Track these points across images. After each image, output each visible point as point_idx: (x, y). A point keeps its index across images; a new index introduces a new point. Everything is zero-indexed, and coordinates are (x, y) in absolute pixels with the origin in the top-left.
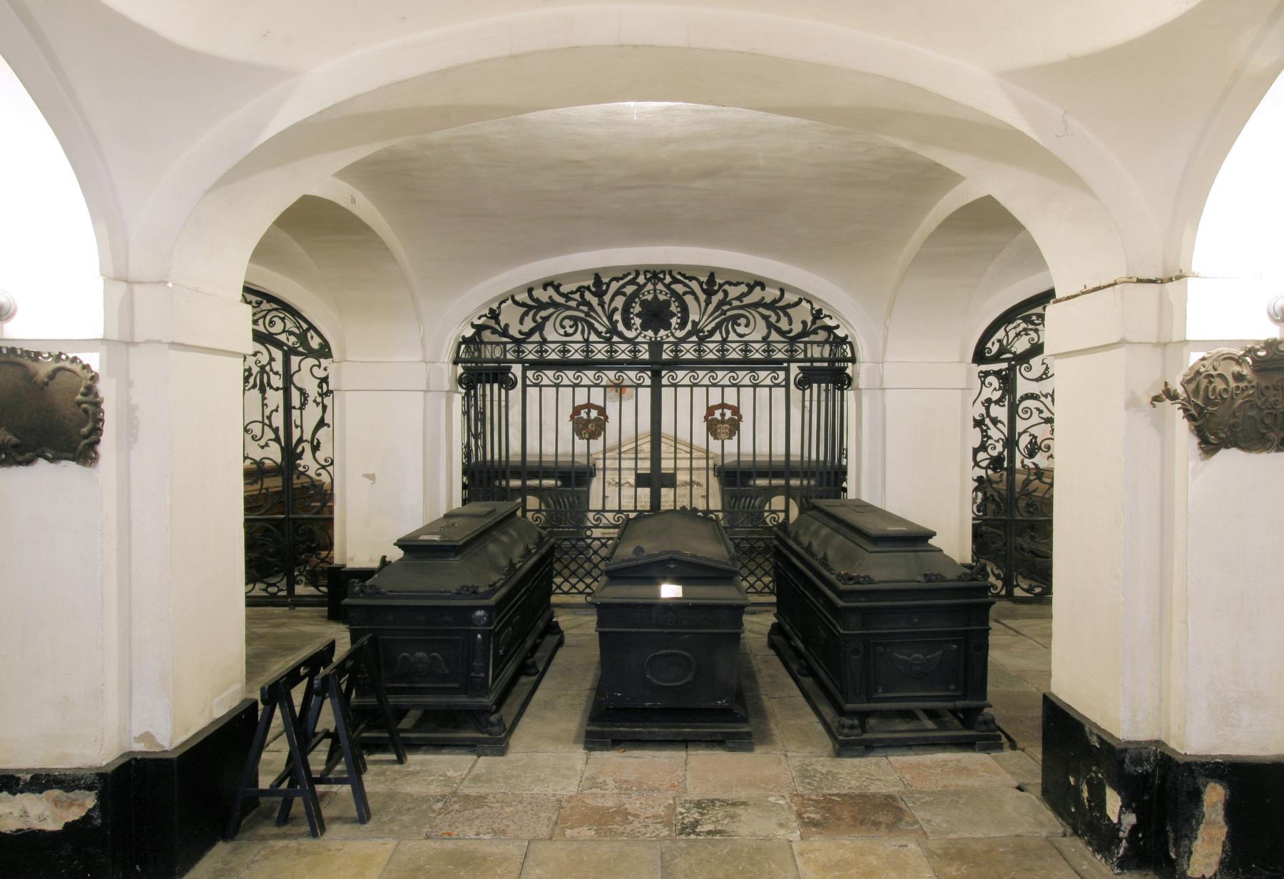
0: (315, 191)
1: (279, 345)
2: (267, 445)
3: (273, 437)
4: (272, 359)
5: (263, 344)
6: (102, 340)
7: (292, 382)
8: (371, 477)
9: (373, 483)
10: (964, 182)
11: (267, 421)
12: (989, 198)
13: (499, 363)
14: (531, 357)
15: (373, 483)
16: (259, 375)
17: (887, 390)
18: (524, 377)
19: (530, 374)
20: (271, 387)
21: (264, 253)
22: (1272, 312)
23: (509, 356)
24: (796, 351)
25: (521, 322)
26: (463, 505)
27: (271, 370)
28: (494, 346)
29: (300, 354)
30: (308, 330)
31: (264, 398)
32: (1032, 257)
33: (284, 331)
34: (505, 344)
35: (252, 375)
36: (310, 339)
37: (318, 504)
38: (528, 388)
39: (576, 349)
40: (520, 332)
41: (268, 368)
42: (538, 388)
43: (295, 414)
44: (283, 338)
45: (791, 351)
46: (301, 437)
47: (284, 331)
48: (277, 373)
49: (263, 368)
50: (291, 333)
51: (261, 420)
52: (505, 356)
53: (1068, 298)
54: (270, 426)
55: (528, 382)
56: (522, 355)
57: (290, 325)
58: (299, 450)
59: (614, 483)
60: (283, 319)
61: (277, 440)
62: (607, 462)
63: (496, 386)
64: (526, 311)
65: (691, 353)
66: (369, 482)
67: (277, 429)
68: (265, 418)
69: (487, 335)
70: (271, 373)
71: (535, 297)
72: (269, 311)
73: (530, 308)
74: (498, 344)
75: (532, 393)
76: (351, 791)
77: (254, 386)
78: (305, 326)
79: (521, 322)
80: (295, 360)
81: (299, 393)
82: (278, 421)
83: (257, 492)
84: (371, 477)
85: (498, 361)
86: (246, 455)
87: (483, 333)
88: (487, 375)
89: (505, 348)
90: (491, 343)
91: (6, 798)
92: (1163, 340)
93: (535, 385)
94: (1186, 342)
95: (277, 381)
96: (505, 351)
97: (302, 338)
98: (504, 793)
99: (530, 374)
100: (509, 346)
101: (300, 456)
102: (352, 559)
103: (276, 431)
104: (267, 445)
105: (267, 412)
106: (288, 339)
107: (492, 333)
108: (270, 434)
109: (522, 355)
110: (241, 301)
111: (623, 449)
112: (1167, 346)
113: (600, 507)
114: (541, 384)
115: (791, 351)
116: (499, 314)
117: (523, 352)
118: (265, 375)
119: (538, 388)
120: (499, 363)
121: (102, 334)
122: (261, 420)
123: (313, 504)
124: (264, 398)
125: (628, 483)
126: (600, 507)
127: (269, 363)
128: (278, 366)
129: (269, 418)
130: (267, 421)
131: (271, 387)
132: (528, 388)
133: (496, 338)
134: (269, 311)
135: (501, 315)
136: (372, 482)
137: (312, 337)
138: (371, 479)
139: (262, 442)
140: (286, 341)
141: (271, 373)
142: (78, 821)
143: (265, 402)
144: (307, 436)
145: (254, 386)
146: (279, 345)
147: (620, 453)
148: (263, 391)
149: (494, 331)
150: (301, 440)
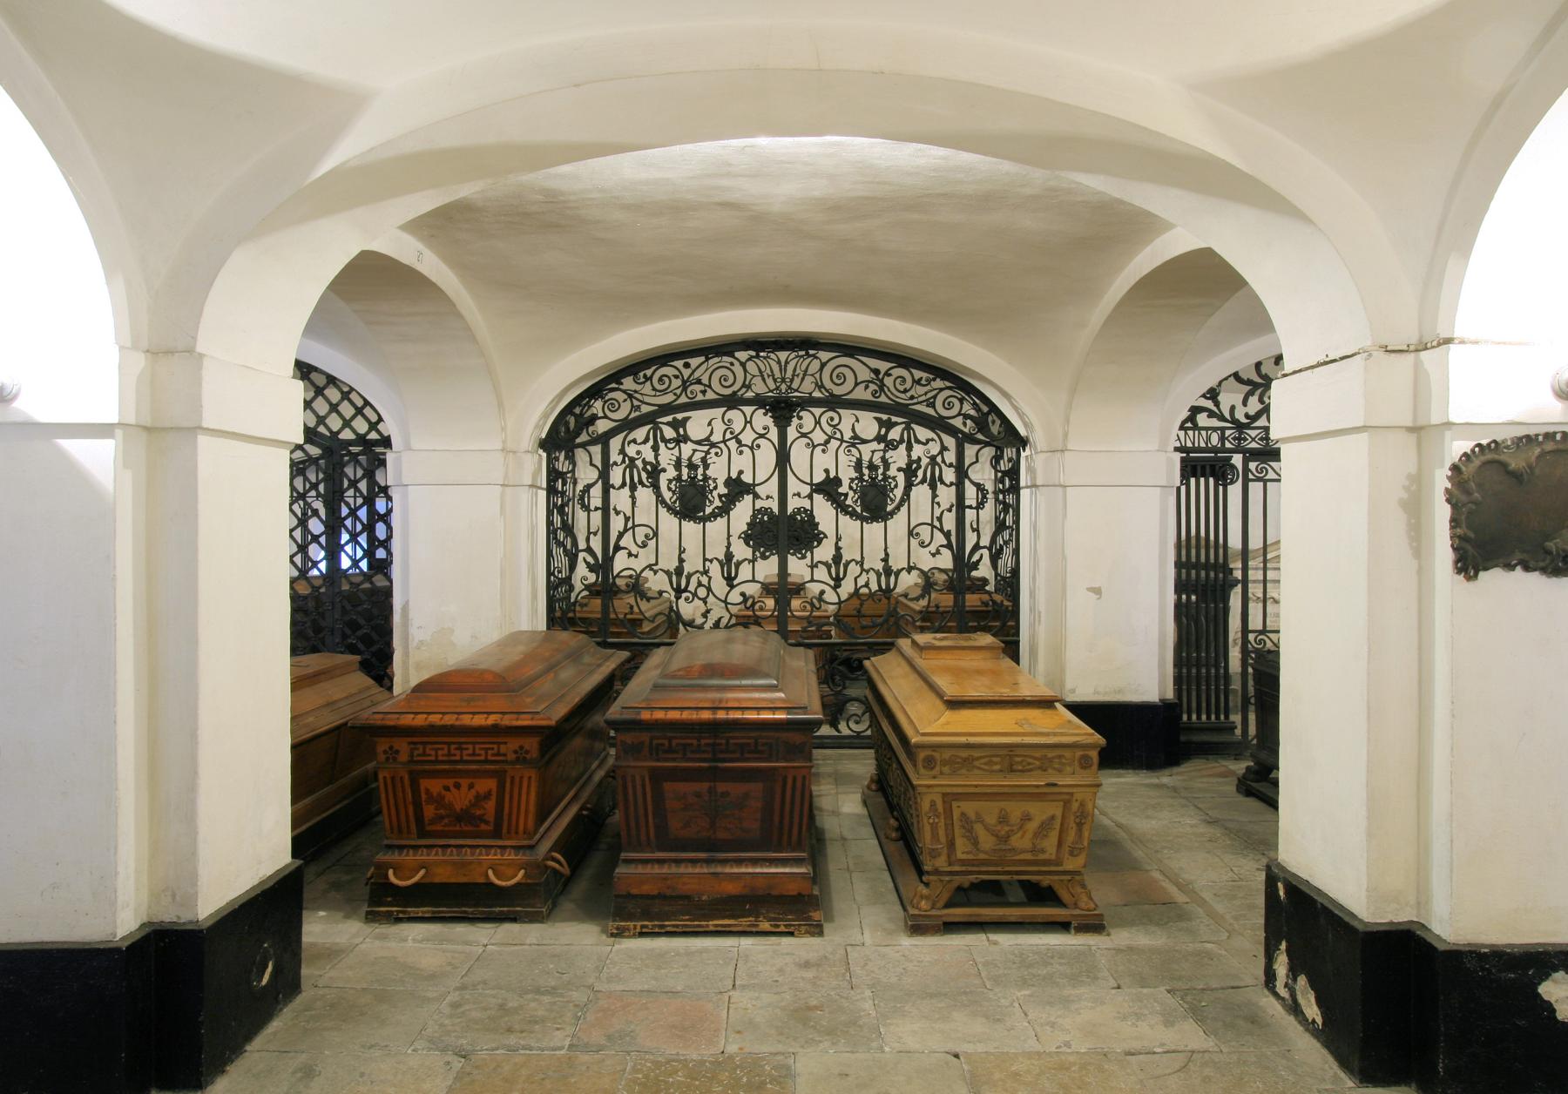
0: (375, 246)
1: (953, 431)
2: (938, 552)
3: (945, 542)
4: (944, 449)
5: (933, 430)
6: (120, 424)
7: (967, 476)
8: (1097, 591)
9: (1098, 599)
10: (1174, 231)
11: (937, 524)
12: (1208, 253)
13: (1216, 453)
14: (1254, 445)
15: (1098, 599)
16: (628, 470)
17: (410, 487)
18: (1246, 470)
19: (1252, 465)
20: (942, 482)
21: (320, 323)
22: (1559, 392)
23: (1228, 445)
24: (1234, 439)
25: (1245, 403)
26: (548, 628)
27: (944, 461)
28: (1209, 432)
29: (978, 442)
30: (989, 413)
31: (934, 496)
32: (1261, 323)
33: (959, 414)
34: (1223, 429)
35: (920, 467)
36: (990, 424)
37: (997, 624)
38: (1250, 483)
39: (1253, 436)
40: (1247, 416)
41: (939, 459)
42: (1262, 483)
43: (970, 515)
44: (958, 423)
45: (1239, 439)
46: (978, 543)
47: (959, 414)
48: (951, 465)
49: (933, 458)
50: (966, 416)
51: (930, 522)
52: (1223, 444)
53: (1295, 372)
54: (941, 530)
55: (1251, 476)
56: (1244, 444)
57: (968, 408)
58: (975, 558)
59: (1255, 598)
60: (961, 401)
61: (949, 546)
62: (1269, 573)
63: (1211, 480)
64: (1251, 390)
65: (1250, 437)
66: (1094, 596)
67: (949, 531)
68: (935, 519)
69: (1202, 419)
70: (943, 465)
71: (1263, 373)
72: (941, 390)
73: (1255, 386)
74: (1215, 429)
75: (1255, 489)
76: (303, 966)
77: (923, 481)
78: (985, 409)
79: (1245, 403)
80: (970, 450)
81: (975, 489)
82: (949, 522)
83: (770, 613)
84: (1097, 591)
85: (1214, 450)
86: (912, 564)
87: (1198, 416)
88: (1203, 467)
89: (1223, 434)
90: (1207, 429)
91: (1563, 978)
92: (1420, 423)
93: (1258, 479)
94: (1449, 425)
95: (950, 475)
96: (1222, 439)
97: (982, 424)
98: (636, 968)
99: (1252, 465)
100: (1228, 433)
101: (975, 566)
102: (1073, 691)
103: (947, 535)
104: (938, 552)
105: (937, 513)
106: (965, 424)
107: (1209, 417)
108: (940, 539)
109: (1244, 444)
110: (294, 377)
111: (1269, 556)
112: (1422, 432)
113: (1260, 627)
114: (1266, 478)
115: (1239, 439)
116: (1218, 394)
117: (1245, 439)
118: (937, 468)
119: (1262, 483)
120: (1216, 453)
121: (117, 418)
122: (930, 522)
123: (990, 624)
124: (934, 496)
125: (1273, 598)
126: (1260, 627)
127: (941, 453)
128: (951, 457)
129: (940, 519)
130: (937, 524)
131: (942, 482)
132: (1250, 483)
133: (1215, 423)
134: (941, 390)
135: (1221, 394)
136: (1098, 596)
137: (993, 422)
138: (1097, 594)
139: (933, 548)
140: (962, 428)
141: (943, 465)
142: (1542, 998)
143: (936, 500)
144: (985, 541)
145: (923, 481)
146: (953, 431)
147: (1265, 561)
148: (933, 487)
149: (1211, 414)
150: (977, 547)
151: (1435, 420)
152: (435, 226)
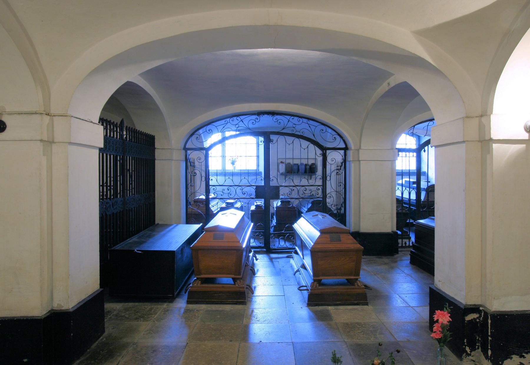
32: (425, 107)
94: (491, 139)
151: (487, 138)
152: (149, 74)
